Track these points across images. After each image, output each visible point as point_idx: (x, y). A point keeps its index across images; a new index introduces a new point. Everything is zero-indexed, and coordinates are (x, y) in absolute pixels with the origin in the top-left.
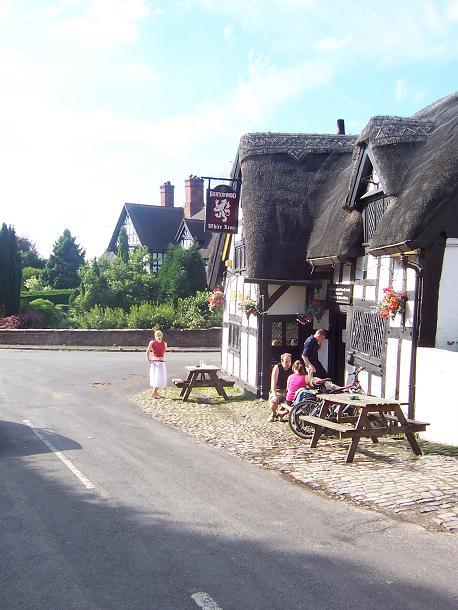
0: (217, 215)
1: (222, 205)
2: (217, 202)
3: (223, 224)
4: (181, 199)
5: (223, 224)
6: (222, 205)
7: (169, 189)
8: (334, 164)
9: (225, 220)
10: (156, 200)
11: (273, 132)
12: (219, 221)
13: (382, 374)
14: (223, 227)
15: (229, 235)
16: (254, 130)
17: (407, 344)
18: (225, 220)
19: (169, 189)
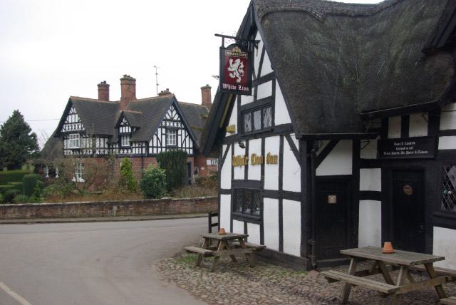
0: (231, 75)
1: (236, 65)
2: (231, 61)
3: (237, 85)
4: (115, 95)
5: (237, 85)
6: (236, 65)
7: (104, 88)
8: (384, 7)
9: (239, 81)
10: (93, 95)
11: (233, 26)
12: (233, 81)
13: (260, 221)
14: (237, 88)
15: (231, 95)
16: (75, 95)
17: (268, 186)
18: (239, 81)
19: (104, 88)
